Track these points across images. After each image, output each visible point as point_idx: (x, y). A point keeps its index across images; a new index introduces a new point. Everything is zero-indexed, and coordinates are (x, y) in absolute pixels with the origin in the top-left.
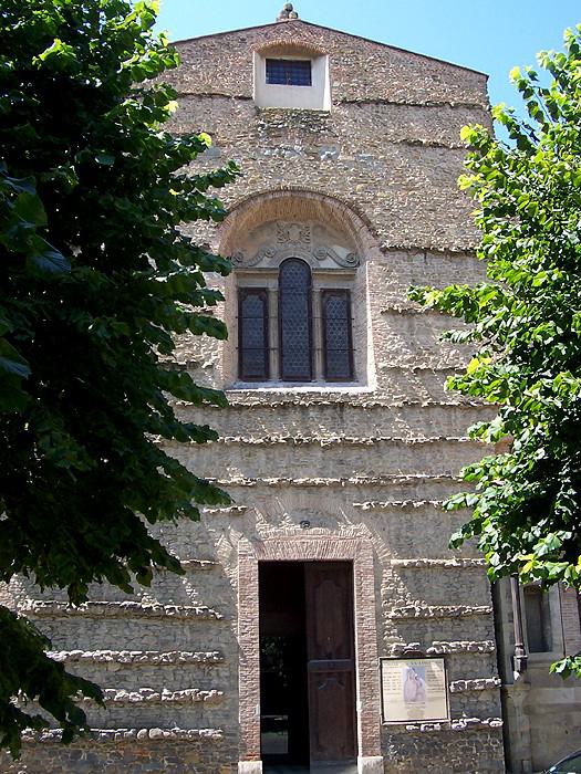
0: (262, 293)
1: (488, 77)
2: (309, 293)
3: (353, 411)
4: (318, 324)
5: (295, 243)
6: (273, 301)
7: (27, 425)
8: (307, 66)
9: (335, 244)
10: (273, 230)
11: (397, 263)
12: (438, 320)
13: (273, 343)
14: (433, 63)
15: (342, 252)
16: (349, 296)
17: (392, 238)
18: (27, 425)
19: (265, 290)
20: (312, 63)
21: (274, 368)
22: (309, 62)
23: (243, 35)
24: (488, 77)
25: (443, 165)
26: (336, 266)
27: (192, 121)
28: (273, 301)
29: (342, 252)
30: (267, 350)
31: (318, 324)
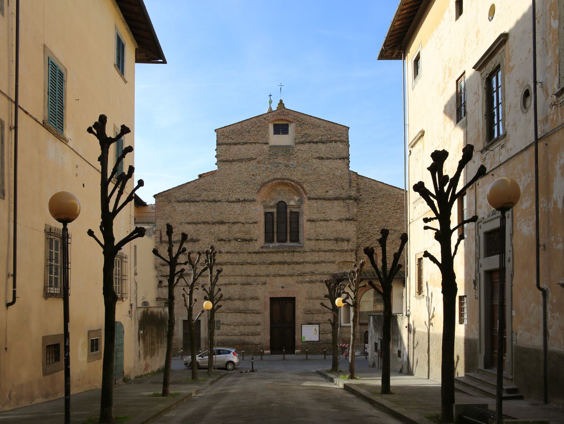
0: (272, 213)
1: (349, 128)
2: (286, 213)
3: (297, 253)
4: (288, 223)
5: (282, 196)
6: (275, 216)
7: (103, 228)
8: (287, 126)
9: (295, 195)
10: (275, 191)
11: (313, 204)
12: (324, 223)
13: (275, 230)
14: (330, 123)
15: (297, 198)
16: (298, 214)
17: (312, 195)
18: (103, 228)
19: (273, 213)
20: (289, 125)
21: (275, 238)
22: (288, 124)
23: (265, 116)
24: (349, 128)
25: (330, 166)
26: (296, 204)
27: (249, 153)
28: (275, 216)
29: (297, 198)
30: (273, 232)
31: (288, 223)
